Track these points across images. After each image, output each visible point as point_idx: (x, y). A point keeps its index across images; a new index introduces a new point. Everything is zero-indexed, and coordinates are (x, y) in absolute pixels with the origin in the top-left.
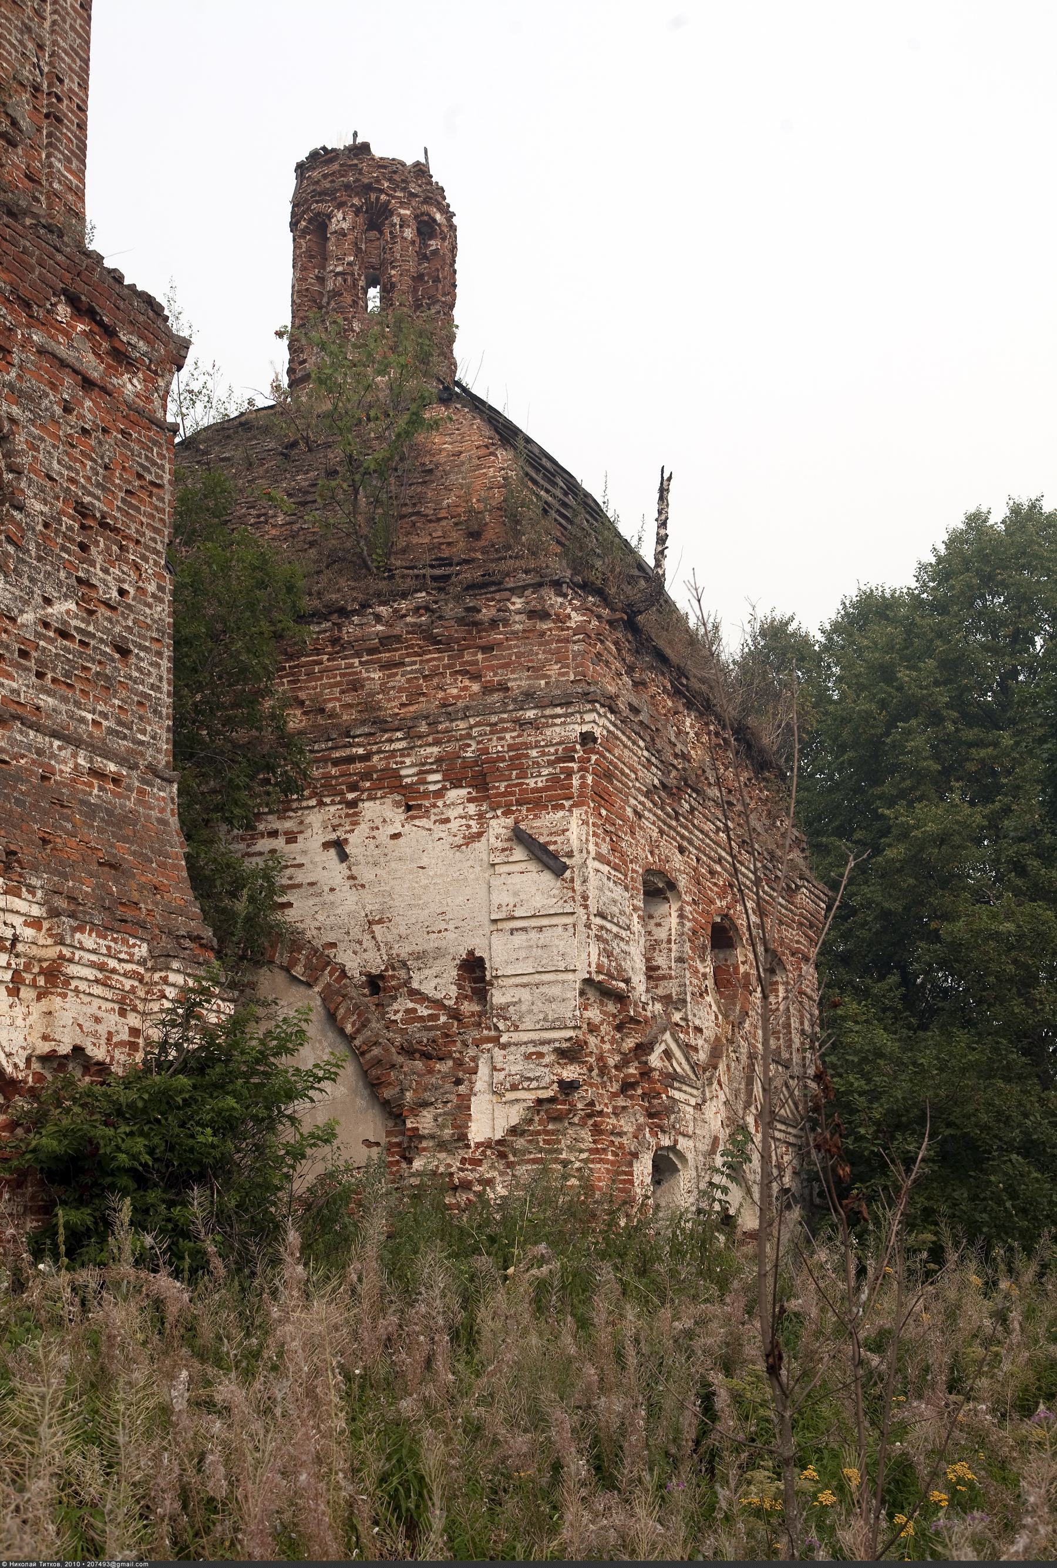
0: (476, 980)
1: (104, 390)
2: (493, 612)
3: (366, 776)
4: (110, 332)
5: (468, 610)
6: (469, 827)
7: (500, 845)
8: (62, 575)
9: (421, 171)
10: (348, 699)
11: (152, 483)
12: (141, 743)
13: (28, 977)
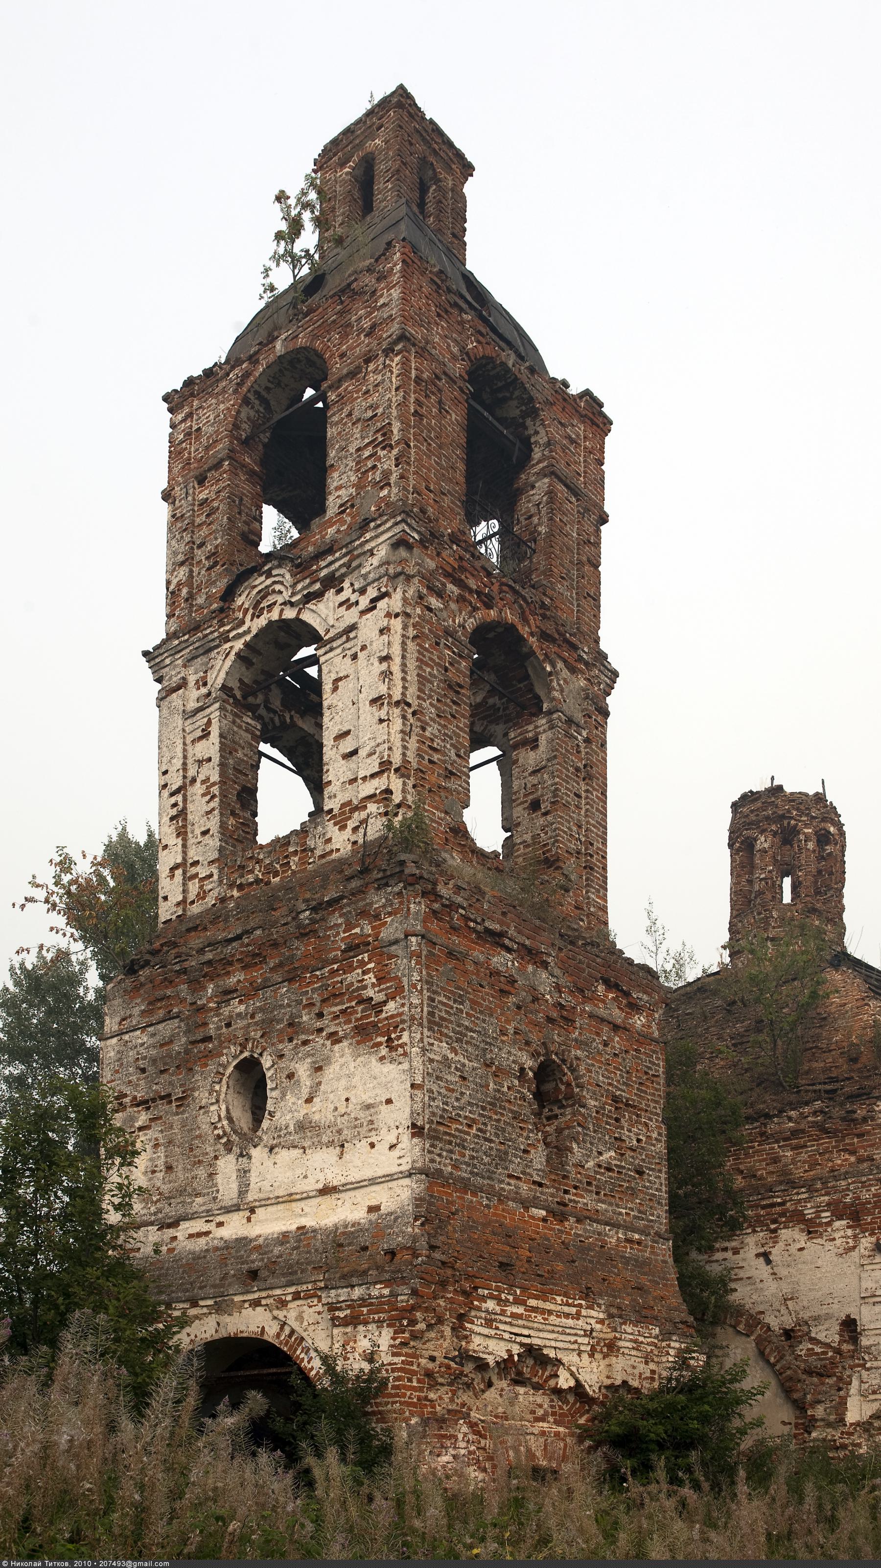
0: (852, 1331)
1: (625, 1029)
2: (865, 1112)
3: (783, 1214)
4: (627, 994)
5: (848, 1112)
6: (847, 1243)
7: (867, 1253)
8: (607, 1137)
9: (820, 798)
10: (771, 1168)
11: (653, 1075)
12: (652, 1221)
13: (598, 1348)
